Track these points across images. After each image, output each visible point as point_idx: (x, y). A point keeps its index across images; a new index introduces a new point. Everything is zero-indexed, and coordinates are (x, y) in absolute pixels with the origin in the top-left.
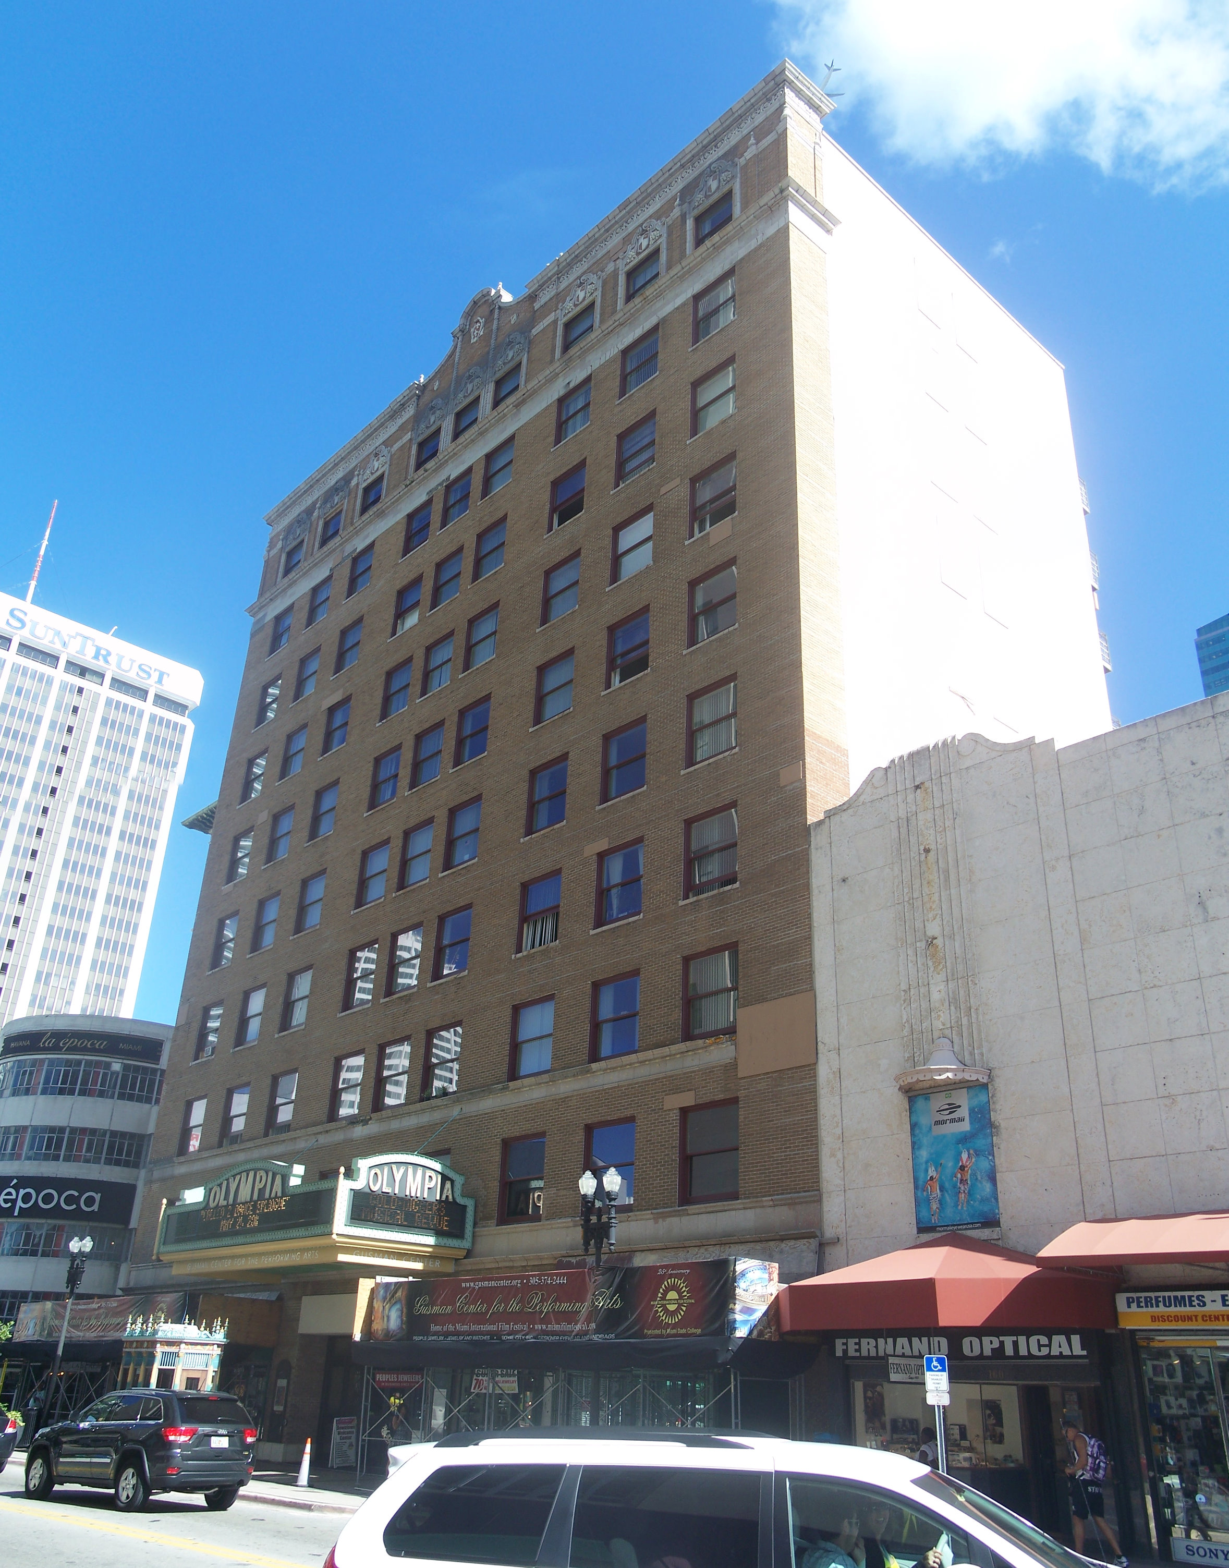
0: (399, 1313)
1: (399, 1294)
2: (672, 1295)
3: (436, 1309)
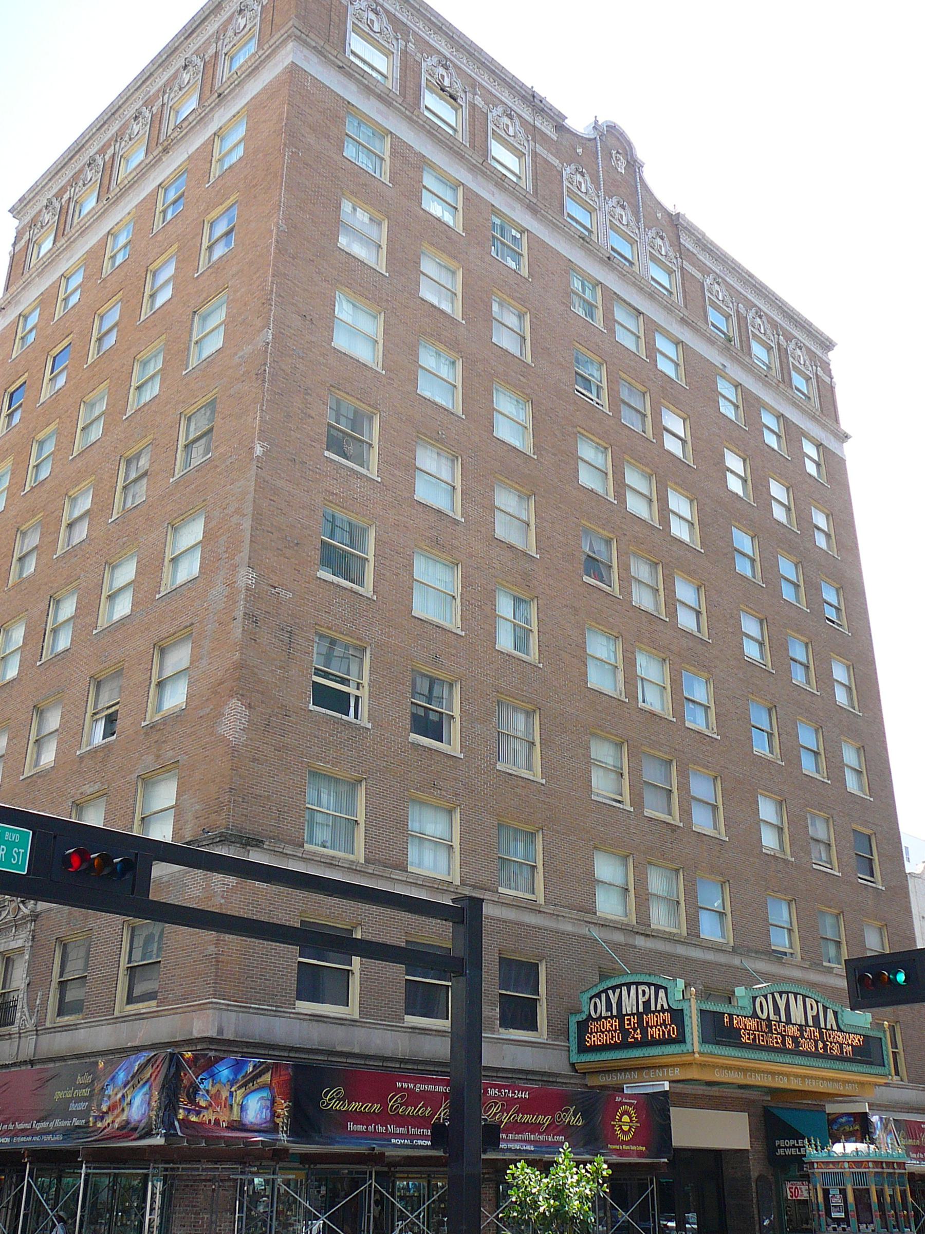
0: (268, 1103)
1: (267, 1078)
2: (626, 1118)
3: (355, 1106)
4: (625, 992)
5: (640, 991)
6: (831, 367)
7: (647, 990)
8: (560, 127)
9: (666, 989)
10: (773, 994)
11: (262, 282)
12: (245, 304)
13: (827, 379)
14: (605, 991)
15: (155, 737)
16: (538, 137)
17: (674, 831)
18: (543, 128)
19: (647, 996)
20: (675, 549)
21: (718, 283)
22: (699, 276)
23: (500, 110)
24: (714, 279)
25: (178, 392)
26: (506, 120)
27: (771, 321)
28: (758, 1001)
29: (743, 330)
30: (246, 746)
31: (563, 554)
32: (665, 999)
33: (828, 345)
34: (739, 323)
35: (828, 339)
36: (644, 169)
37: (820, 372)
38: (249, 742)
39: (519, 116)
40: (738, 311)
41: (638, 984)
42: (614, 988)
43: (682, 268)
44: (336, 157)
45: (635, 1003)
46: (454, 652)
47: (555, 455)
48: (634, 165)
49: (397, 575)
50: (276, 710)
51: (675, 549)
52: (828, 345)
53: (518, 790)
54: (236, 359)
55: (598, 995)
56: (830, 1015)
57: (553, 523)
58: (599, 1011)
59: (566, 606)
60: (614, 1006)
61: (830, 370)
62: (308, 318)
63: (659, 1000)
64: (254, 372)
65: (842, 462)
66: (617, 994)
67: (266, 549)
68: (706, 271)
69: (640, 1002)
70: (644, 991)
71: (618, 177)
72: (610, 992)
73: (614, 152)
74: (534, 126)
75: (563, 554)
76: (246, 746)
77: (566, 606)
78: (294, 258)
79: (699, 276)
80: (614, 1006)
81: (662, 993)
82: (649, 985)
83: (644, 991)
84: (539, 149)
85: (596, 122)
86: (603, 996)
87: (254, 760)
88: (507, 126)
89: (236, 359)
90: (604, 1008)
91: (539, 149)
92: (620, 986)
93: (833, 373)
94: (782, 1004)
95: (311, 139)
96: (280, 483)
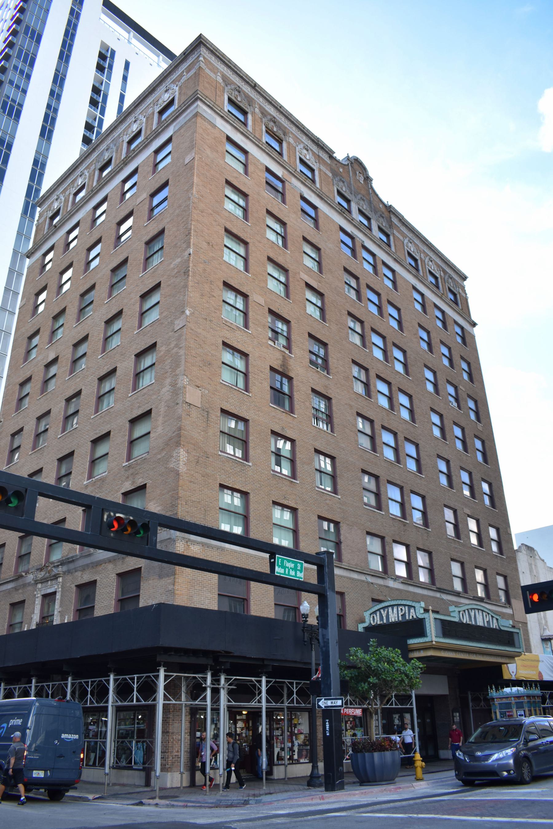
4: (390, 610)
5: (399, 609)
6: (466, 289)
7: (403, 608)
8: (331, 157)
9: (414, 607)
10: (468, 610)
11: (185, 225)
12: (176, 237)
13: (464, 295)
14: (379, 610)
15: (131, 471)
16: (321, 161)
17: (405, 525)
18: (323, 157)
19: (403, 612)
20: (397, 377)
21: (411, 243)
22: (401, 238)
23: (301, 146)
24: (409, 241)
25: (137, 286)
26: (305, 151)
27: (437, 264)
28: (461, 613)
29: (424, 267)
30: (186, 473)
31: (344, 377)
32: (414, 613)
33: (464, 278)
34: (421, 263)
35: (463, 274)
36: (373, 182)
37: (461, 291)
38: (188, 471)
39: (312, 150)
40: (421, 258)
41: (398, 605)
42: (384, 608)
43: (393, 234)
44: (222, 162)
45: (396, 616)
46: (292, 426)
47: (337, 325)
48: (368, 179)
49: (261, 383)
50: (202, 454)
51: (397, 377)
52: (464, 278)
53: (328, 502)
54: (172, 266)
55: (375, 612)
56: (495, 621)
57: (338, 360)
58: (376, 621)
59: (346, 404)
60: (385, 618)
61: (465, 291)
62: (211, 244)
63: (411, 614)
64: (183, 271)
65: (473, 337)
66: (386, 612)
67: (194, 366)
68: (405, 236)
69: (400, 615)
70: (401, 609)
71: (360, 185)
72: (382, 611)
73: (358, 173)
74: (319, 156)
75: (344, 377)
76: (186, 473)
77: (346, 404)
78: (202, 212)
79: (401, 238)
80: (385, 618)
81: (412, 610)
82: (405, 605)
83: (401, 609)
84: (322, 168)
85: (348, 156)
86: (378, 613)
87: (191, 482)
88: (306, 154)
89: (172, 266)
90: (378, 619)
91: (322, 168)
92: (387, 607)
93: (467, 292)
94: (472, 614)
95: (208, 151)
96: (199, 331)
